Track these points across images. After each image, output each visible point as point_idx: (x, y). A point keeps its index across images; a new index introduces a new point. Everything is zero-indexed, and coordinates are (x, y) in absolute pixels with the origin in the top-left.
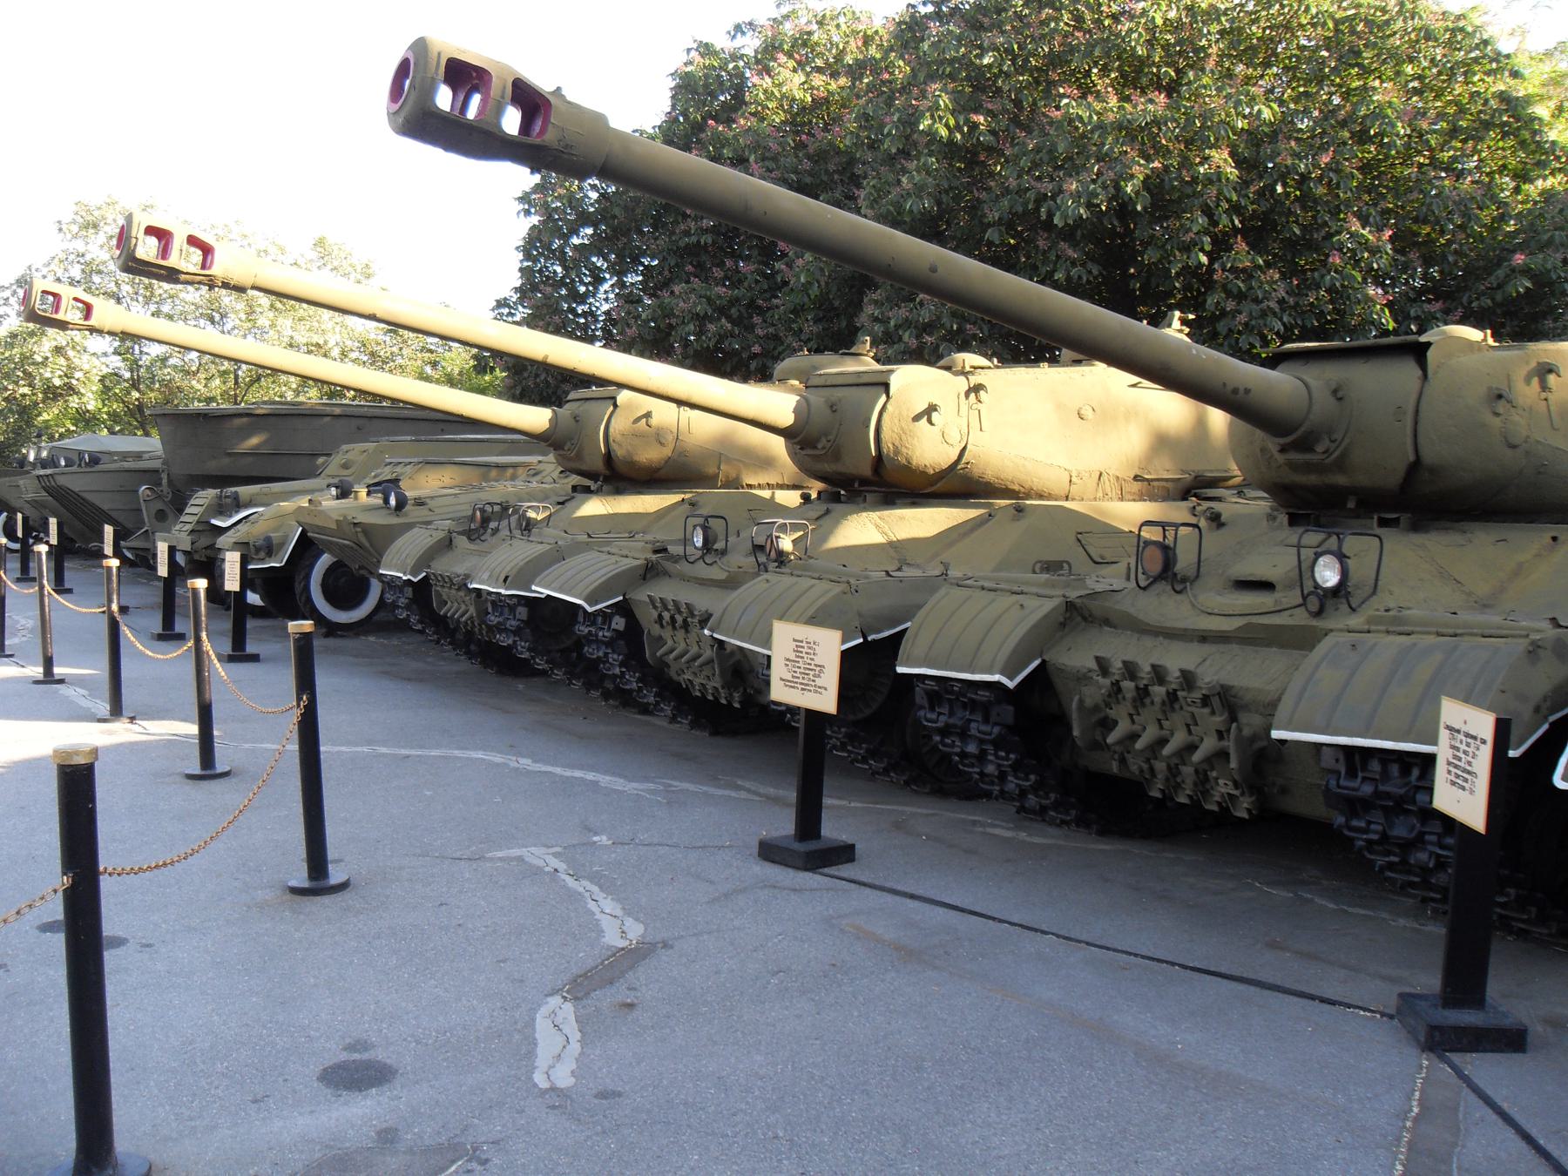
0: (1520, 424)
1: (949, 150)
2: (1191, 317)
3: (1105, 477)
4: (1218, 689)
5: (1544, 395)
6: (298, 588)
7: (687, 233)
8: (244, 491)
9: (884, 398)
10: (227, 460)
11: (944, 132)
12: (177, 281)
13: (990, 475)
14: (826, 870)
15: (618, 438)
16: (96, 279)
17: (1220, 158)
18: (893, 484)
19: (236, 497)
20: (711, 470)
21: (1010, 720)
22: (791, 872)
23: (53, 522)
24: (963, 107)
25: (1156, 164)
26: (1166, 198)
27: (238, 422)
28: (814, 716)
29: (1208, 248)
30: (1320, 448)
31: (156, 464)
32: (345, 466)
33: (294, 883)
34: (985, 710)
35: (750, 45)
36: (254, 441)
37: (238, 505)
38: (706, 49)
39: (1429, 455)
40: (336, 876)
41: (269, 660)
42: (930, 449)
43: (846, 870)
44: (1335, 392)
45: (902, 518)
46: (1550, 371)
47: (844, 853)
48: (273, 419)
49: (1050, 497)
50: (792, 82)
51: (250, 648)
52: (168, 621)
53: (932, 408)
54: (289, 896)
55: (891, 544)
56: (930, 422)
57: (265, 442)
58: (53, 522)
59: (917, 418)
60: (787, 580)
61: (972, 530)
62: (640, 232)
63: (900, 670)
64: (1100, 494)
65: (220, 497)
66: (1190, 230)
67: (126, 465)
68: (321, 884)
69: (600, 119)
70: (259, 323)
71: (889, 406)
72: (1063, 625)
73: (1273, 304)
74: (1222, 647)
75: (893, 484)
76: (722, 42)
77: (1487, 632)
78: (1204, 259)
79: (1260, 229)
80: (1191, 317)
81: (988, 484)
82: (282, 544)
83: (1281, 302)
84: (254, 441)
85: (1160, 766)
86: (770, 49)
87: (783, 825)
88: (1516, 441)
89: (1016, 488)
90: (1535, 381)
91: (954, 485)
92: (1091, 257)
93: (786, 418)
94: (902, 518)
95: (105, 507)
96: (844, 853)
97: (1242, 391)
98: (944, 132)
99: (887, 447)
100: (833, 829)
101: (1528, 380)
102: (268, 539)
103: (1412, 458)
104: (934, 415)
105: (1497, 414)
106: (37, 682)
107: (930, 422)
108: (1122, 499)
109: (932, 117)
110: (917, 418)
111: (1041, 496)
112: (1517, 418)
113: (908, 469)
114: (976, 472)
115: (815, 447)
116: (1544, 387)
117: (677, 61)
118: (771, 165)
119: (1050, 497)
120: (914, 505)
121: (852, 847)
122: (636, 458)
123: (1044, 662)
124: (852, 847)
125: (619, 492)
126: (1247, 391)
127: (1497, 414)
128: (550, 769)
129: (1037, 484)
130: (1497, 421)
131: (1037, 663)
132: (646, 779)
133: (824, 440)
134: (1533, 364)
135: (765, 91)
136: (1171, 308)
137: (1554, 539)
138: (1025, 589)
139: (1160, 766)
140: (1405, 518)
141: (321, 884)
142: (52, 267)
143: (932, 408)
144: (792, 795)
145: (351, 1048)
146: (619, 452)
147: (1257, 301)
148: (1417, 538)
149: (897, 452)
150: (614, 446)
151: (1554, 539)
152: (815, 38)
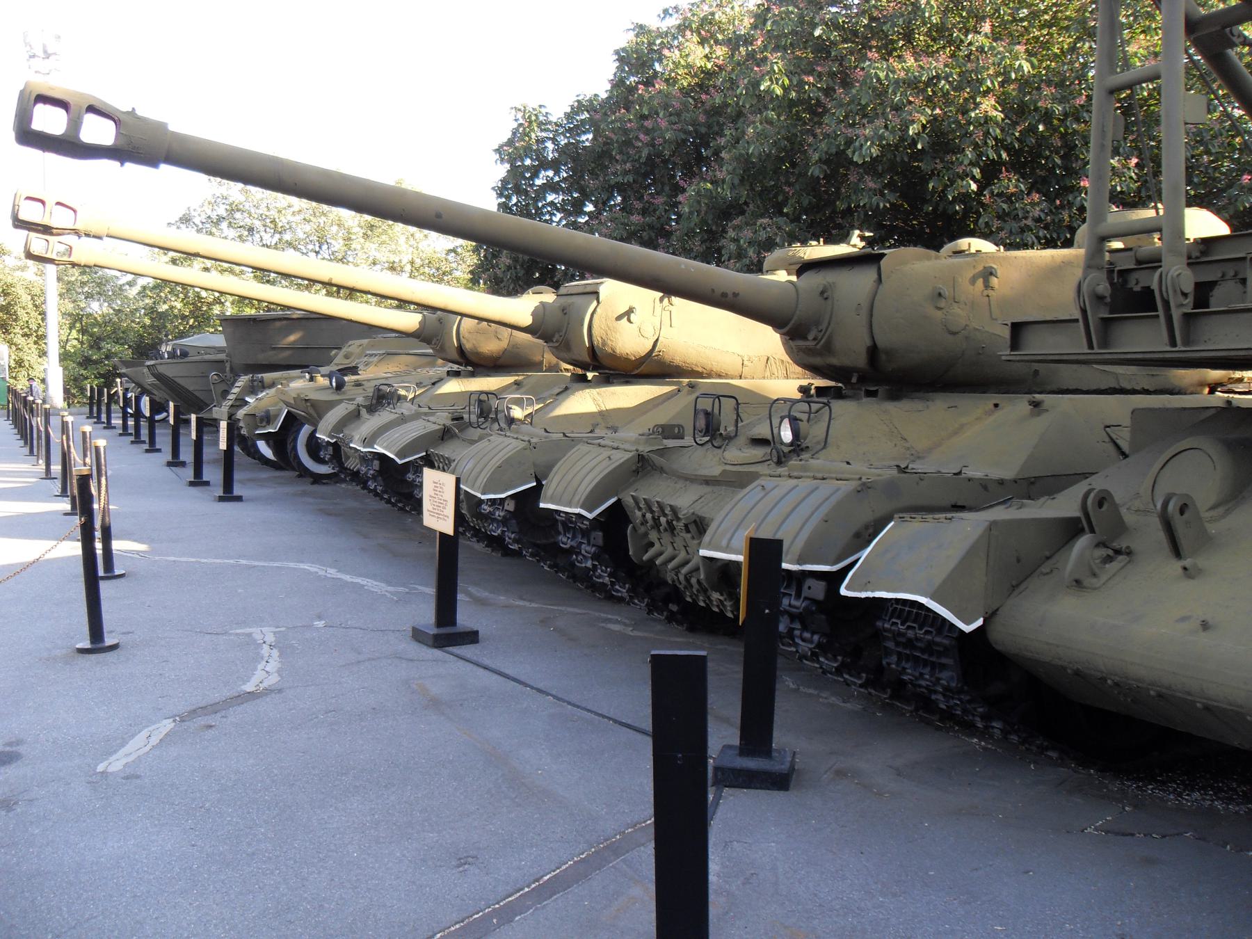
0: (959, 315)
1: (786, 105)
2: (867, 234)
3: (771, 360)
4: (693, 518)
5: (986, 293)
6: (289, 447)
7: (615, 174)
8: (268, 376)
9: (595, 303)
10: (271, 353)
11: (779, 91)
12: (52, 234)
13: (678, 360)
14: (450, 649)
15: (467, 335)
16: (238, 215)
17: (988, 106)
18: (609, 368)
19: (262, 381)
20: (537, 358)
21: (600, 542)
22: (424, 648)
23: (171, 404)
24: (796, 70)
25: (937, 111)
26: (942, 141)
27: (278, 324)
28: (443, 536)
29: (978, 176)
30: (811, 337)
31: (222, 356)
32: (347, 357)
33: (79, 646)
34: (585, 534)
35: (673, 21)
36: (292, 338)
37: (263, 386)
38: (641, 29)
39: (881, 342)
40: (109, 641)
41: (251, 500)
42: (629, 341)
43: (467, 650)
44: (822, 293)
45: (614, 393)
46: (991, 274)
47: (471, 637)
48: (304, 322)
49: (727, 376)
50: (697, 55)
51: (237, 491)
52: (198, 471)
53: (630, 311)
54: (77, 655)
55: (601, 414)
56: (629, 320)
57: (302, 338)
58: (171, 404)
59: (619, 318)
60: (501, 439)
61: (658, 405)
62: (525, 178)
63: (542, 505)
64: (768, 374)
65: (252, 381)
66: (961, 163)
67: (207, 357)
68: (100, 645)
69: (161, 127)
70: (353, 246)
71: (598, 310)
72: (637, 472)
73: (1029, 222)
74: (716, 488)
75: (609, 368)
76: (653, 23)
77: (839, 476)
78: (974, 187)
79: (1026, 160)
80: (867, 234)
81: (678, 367)
82: (277, 416)
83: (1039, 220)
84: (292, 338)
85: (682, 578)
86: (682, 28)
87: (426, 615)
88: (954, 329)
89: (700, 370)
90: (980, 282)
91: (650, 368)
92: (891, 185)
93: (527, 320)
94: (614, 393)
95: (191, 389)
96: (471, 637)
97: (730, 295)
98: (779, 91)
99: (597, 340)
100: (465, 618)
101: (973, 281)
102: (268, 412)
103: (869, 343)
104: (633, 316)
105: (940, 309)
106: (66, 514)
107: (629, 320)
108: (787, 377)
109: (771, 80)
110: (619, 318)
111: (720, 376)
112: (959, 311)
113: (613, 356)
114: (668, 358)
115: (805, 338)
116: (987, 285)
117: (625, 39)
118: (674, 119)
119: (727, 376)
120: (627, 383)
121: (476, 633)
122: (481, 350)
123: (619, 500)
124: (476, 633)
125: (473, 375)
126: (735, 295)
127: (940, 309)
128: (359, 580)
129: (716, 368)
130: (939, 313)
131: (613, 500)
132: (389, 583)
133: (557, 336)
134: (980, 268)
135: (674, 63)
136: (853, 227)
137: (996, 405)
138: (621, 446)
139: (682, 578)
140: (882, 390)
141: (100, 645)
142: (205, 208)
143: (630, 311)
144: (431, 591)
145: (10, 744)
146: (468, 346)
147: (1016, 218)
148: (891, 407)
149: (604, 344)
150: (464, 341)
151: (996, 405)
152: (717, 17)
